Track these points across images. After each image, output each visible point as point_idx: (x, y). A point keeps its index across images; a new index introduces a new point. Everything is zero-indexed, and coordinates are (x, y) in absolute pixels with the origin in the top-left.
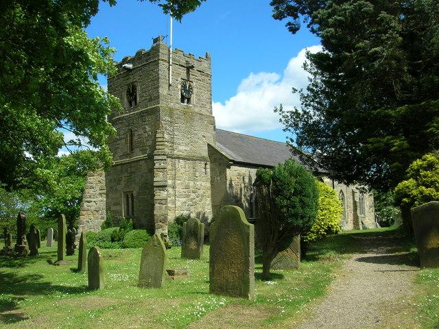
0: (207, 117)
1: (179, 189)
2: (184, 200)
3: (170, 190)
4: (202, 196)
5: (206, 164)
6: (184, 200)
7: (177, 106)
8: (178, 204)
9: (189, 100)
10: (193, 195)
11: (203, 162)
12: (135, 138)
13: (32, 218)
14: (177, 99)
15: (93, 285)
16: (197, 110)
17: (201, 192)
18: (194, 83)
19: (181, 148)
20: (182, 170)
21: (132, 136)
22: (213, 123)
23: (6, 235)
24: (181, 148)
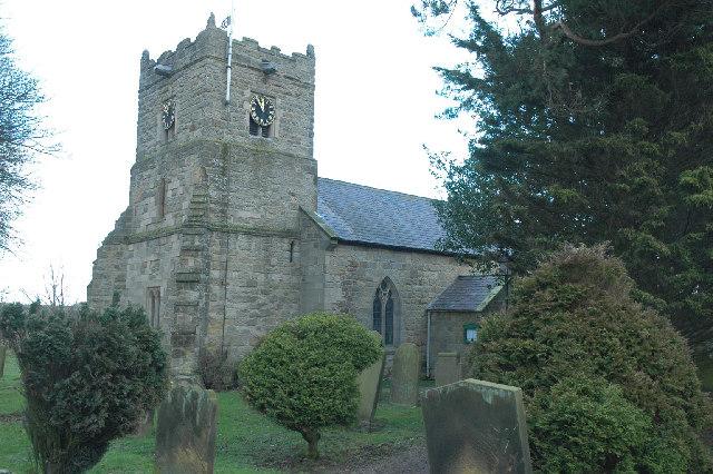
0: (301, 160)
1: (235, 287)
2: (244, 306)
3: (216, 289)
4: (283, 300)
5: (292, 245)
6: (244, 306)
7: (239, 139)
8: (231, 313)
9: (266, 131)
10: (262, 299)
11: (286, 241)
12: (169, 194)
13: (518, 277)
14: (242, 127)
15: (503, 14)
16: (282, 147)
17: (279, 293)
18: (279, 101)
19: (243, 214)
20: (243, 254)
21: (164, 191)
22: (313, 170)
23: (486, 261)
24: (243, 214)
